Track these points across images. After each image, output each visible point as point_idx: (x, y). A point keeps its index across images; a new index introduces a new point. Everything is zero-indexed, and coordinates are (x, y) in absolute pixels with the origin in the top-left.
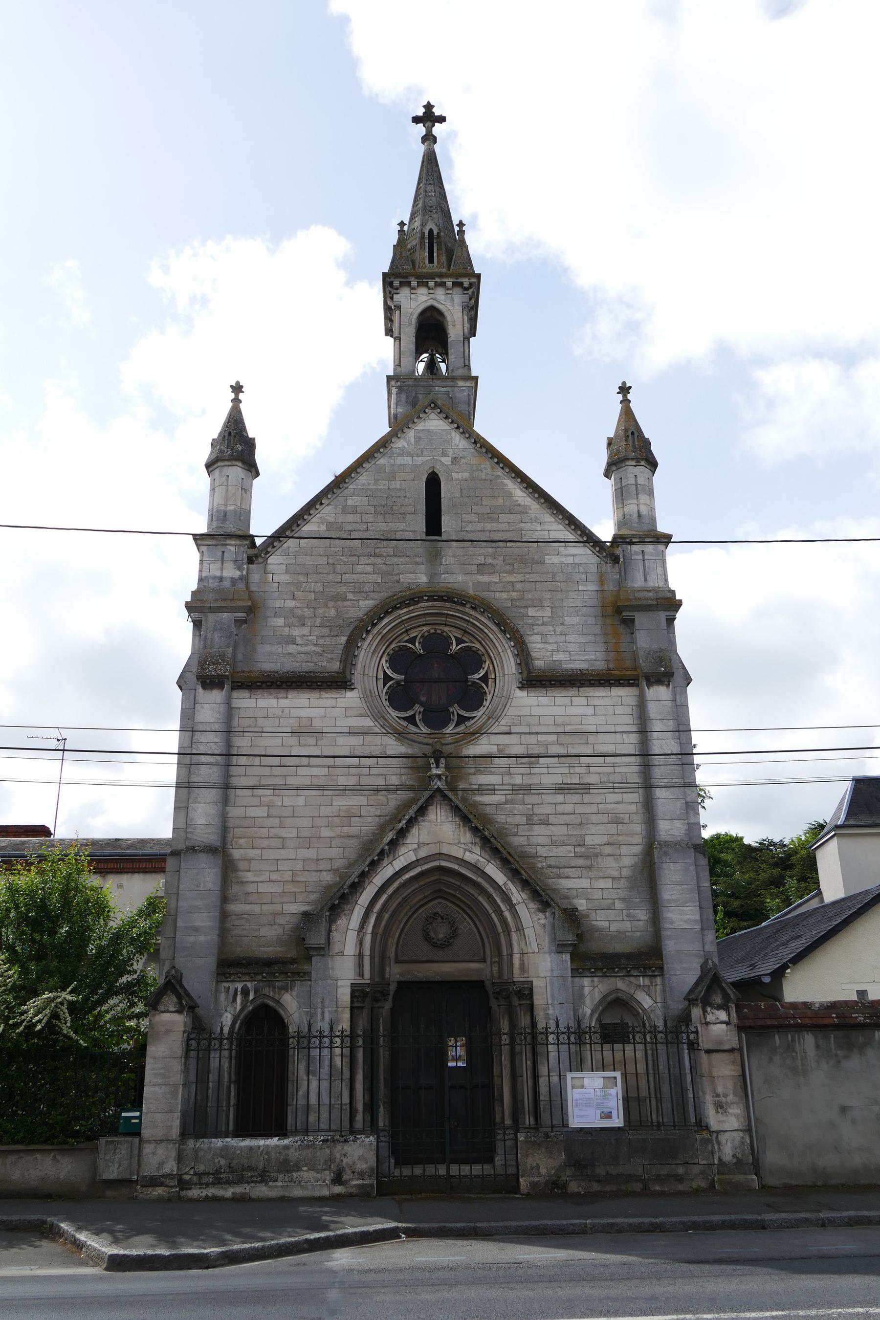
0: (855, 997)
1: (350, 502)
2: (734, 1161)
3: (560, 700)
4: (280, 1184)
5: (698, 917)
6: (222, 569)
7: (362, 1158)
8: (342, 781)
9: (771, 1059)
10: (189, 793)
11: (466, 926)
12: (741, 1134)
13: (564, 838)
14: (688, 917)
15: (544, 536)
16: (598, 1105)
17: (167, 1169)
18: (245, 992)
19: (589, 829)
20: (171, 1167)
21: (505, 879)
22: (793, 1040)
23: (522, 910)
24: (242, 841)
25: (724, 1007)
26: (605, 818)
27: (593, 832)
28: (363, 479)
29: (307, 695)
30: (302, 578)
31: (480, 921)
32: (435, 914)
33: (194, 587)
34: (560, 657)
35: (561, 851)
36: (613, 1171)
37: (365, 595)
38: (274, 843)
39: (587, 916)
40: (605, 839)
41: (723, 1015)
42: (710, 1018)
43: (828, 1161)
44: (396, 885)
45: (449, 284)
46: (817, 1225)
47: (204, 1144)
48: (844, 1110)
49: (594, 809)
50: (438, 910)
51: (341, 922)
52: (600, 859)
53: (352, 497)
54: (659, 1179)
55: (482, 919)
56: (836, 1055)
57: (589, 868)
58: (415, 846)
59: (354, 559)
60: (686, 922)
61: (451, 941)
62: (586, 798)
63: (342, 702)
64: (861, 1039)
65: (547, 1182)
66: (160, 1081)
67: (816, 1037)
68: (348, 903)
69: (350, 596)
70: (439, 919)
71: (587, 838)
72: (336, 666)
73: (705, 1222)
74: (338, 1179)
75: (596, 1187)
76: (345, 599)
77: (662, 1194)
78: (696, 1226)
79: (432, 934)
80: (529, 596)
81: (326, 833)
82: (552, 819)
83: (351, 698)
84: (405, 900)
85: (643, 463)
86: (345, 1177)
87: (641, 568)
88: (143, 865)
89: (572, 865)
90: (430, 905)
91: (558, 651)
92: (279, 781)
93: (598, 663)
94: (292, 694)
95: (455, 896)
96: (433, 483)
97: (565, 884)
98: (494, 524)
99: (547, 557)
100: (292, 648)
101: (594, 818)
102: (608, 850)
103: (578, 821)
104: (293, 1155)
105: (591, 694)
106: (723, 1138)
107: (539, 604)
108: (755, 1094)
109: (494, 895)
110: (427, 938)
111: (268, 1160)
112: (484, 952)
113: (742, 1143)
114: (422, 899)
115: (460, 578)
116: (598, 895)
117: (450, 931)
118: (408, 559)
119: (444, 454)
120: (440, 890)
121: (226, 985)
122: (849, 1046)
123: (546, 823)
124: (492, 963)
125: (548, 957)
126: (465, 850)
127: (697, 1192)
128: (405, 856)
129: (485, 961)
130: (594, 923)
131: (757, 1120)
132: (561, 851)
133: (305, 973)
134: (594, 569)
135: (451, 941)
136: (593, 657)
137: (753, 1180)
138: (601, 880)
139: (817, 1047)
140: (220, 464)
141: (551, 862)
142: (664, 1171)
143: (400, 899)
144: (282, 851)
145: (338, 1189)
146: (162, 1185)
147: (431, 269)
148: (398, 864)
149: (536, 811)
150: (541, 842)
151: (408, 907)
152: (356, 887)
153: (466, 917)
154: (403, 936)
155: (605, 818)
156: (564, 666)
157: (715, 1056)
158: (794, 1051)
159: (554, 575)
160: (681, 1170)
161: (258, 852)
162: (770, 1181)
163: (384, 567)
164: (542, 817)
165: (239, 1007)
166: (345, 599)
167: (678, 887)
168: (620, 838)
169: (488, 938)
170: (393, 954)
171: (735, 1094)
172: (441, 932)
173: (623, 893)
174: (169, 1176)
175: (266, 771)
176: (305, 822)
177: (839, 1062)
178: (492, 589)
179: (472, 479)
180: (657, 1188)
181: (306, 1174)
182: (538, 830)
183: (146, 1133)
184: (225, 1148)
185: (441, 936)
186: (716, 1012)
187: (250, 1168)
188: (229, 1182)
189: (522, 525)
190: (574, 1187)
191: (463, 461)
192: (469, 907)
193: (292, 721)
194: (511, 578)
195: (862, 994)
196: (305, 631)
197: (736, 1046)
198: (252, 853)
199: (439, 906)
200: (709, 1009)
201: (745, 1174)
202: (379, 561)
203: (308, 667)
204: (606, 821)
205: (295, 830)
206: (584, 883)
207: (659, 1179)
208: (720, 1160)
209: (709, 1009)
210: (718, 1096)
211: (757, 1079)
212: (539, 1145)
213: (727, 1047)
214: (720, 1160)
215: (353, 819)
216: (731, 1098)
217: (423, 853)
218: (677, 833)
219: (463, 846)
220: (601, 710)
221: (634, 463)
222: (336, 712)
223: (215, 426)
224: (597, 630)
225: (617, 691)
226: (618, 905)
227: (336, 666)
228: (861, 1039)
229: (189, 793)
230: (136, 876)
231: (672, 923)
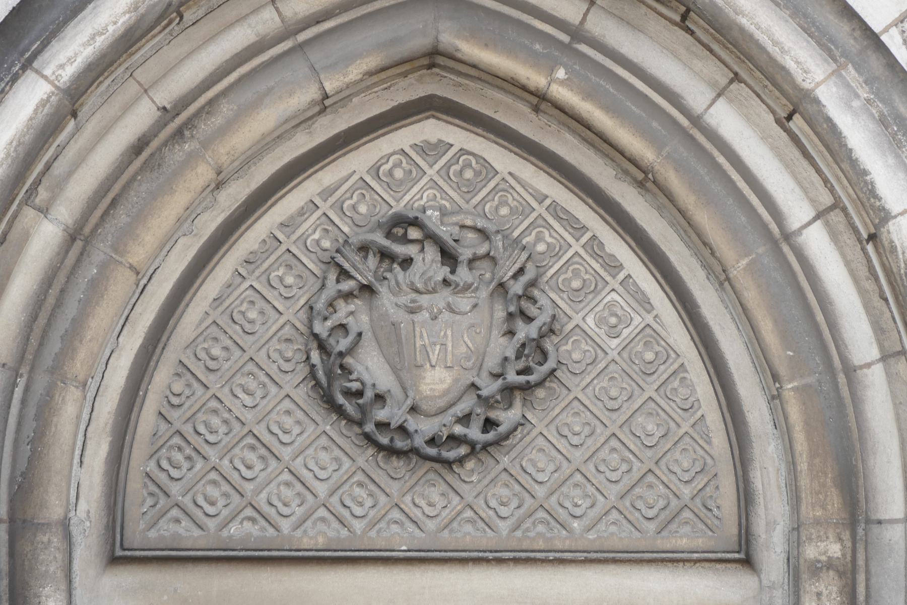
10: (135, 79)
11: (611, 310)
31: (722, 278)
32: (400, 224)
50: (415, 198)
55: (738, 267)
61: (507, 417)
70: (428, 262)
79: (372, 368)
84: (179, 123)
90: (358, 161)
95: (540, 101)
109: (830, 100)
110: (336, 392)
112: (746, 497)
114: (302, 121)
117: (500, 347)
120: (435, 58)
124: (797, 572)
129: (748, 562)
135: (507, 417)
143: (141, 117)
151: (203, 174)
153: (617, 246)
154: (162, 376)
169: (775, 399)
170: (88, 508)
172: (439, 350)
185: (436, 382)
192: (645, 179)
199: (421, 168)
229: (135, 79)
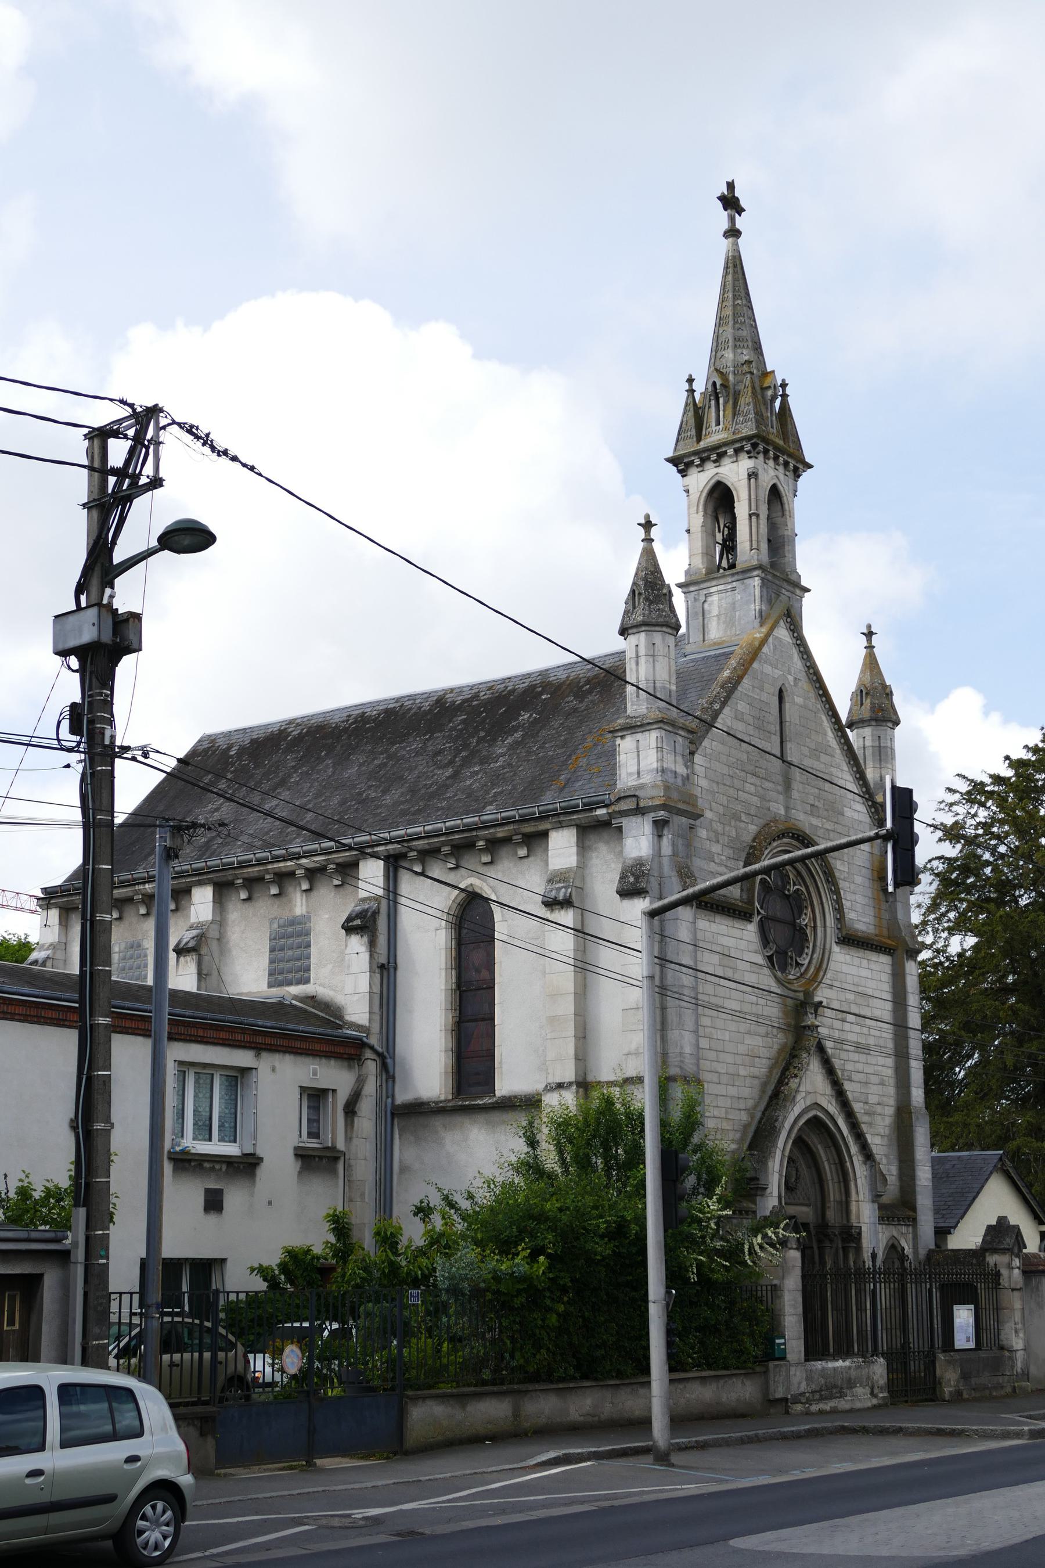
15: (840, 782)
17: (802, 1389)
47: (819, 1365)
86: (876, 1391)
88: (298, 1044)
94: (719, 918)
103: (864, 1080)
104: (853, 1373)
133: (747, 1212)
140: (664, 629)
145: (875, 1401)
147: (743, 424)
174: (803, 1394)
183: (789, 1357)
187: (835, 1386)
190: (965, 1396)
225: (873, 956)
230: (288, 1058)
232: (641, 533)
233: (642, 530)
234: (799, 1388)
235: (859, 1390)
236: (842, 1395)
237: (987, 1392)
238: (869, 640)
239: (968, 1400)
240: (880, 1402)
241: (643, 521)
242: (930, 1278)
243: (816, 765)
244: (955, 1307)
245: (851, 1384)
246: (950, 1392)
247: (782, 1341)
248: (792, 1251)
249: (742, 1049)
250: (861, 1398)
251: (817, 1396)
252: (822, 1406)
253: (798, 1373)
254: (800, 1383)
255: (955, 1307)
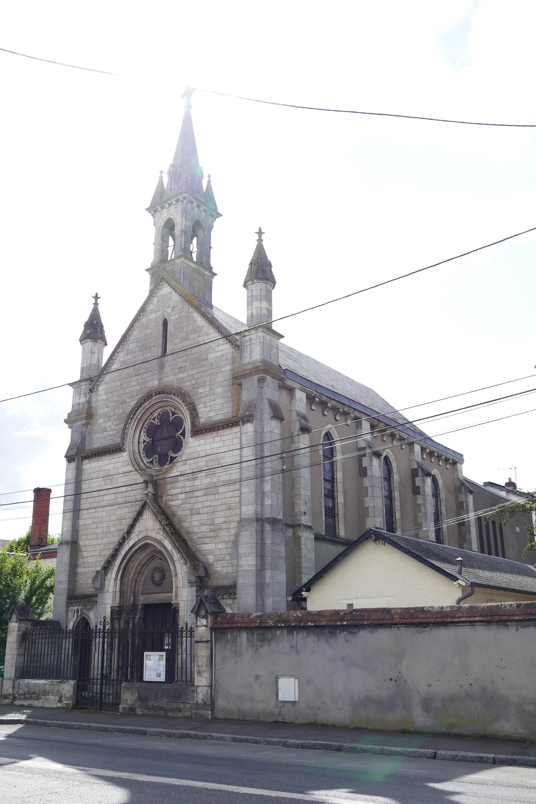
0: (345, 608)
1: (130, 348)
2: (203, 702)
3: (210, 440)
4: (42, 701)
5: (255, 563)
6: (80, 399)
7: (68, 691)
8: (119, 500)
9: (225, 647)
12: (206, 688)
13: (205, 521)
14: (250, 563)
16: (156, 669)
17: (9, 692)
18: (78, 612)
19: (217, 514)
20: (10, 691)
21: (172, 547)
22: (237, 636)
23: (177, 564)
24: (83, 537)
25: (205, 617)
26: (224, 507)
27: (218, 516)
28: (136, 333)
29: (108, 458)
30: (110, 395)
33: (70, 410)
34: (211, 414)
35: (204, 528)
36: (155, 704)
37: (133, 398)
38: (94, 536)
39: (213, 565)
40: (223, 520)
41: (204, 622)
42: (199, 623)
43: (247, 706)
44: (129, 555)
45: (174, 202)
46: (167, 736)
48: (257, 677)
49: (219, 502)
51: (109, 575)
52: (221, 531)
53: (131, 345)
54: (172, 710)
56: (257, 645)
57: (215, 537)
58: (138, 533)
59: (129, 379)
60: (249, 566)
62: (217, 496)
63: (122, 459)
64: (270, 636)
65: (129, 708)
66: (10, 653)
67: (248, 634)
68: (111, 565)
69: (128, 400)
71: (216, 520)
72: (118, 440)
73: (124, 729)
74: (60, 701)
75: (147, 712)
76: (126, 402)
77: (173, 717)
78: (119, 731)
80: (200, 381)
81: (113, 529)
82: (201, 511)
83: (124, 457)
85: (255, 281)
86: (63, 699)
87: (249, 350)
89: (208, 536)
91: (211, 411)
92: (96, 505)
93: (229, 414)
96: (165, 323)
97: (205, 547)
98: (187, 342)
99: (209, 355)
100: (106, 434)
101: (219, 508)
102: (225, 526)
103: (212, 511)
104: (48, 688)
105: (223, 434)
106: (199, 690)
107: (203, 385)
108: (217, 666)
111: (40, 690)
113: (207, 693)
115: (171, 378)
116: (218, 552)
118: (151, 373)
119: (169, 307)
121: (71, 608)
122: (263, 639)
123: (198, 513)
125: (186, 590)
126: (157, 533)
127: (187, 718)
128: (134, 539)
130: (216, 569)
131: (215, 681)
132: (204, 528)
134: (230, 356)
136: (226, 411)
137: (209, 714)
138: (221, 544)
139: (248, 640)
141: (200, 535)
142: (175, 706)
144: (97, 540)
145: (59, 705)
146: (8, 698)
148: (131, 543)
149: (195, 507)
150: (194, 524)
152: (114, 556)
155: (224, 507)
156: (214, 419)
157: (199, 644)
158: (237, 642)
159: (212, 364)
160: (182, 706)
161: (88, 541)
162: (219, 715)
163: (141, 380)
164: (197, 510)
165: (75, 619)
166: (126, 402)
167: (247, 546)
168: (231, 518)
171: (206, 666)
173: (230, 551)
174: (9, 694)
175: (92, 500)
176: (105, 525)
177: (258, 649)
178: (184, 381)
179: (179, 317)
180: (170, 715)
181: (51, 697)
182: (196, 517)
183: (5, 675)
184: (28, 684)
186: (201, 619)
187: (34, 693)
188: (28, 699)
189: (200, 338)
190: (138, 711)
191: (176, 308)
193: (103, 472)
194: (192, 372)
195: (350, 605)
196: (110, 424)
197: (209, 639)
198: (87, 542)
200: (198, 618)
201: (206, 710)
202: (139, 377)
203: (110, 442)
204: (225, 508)
205: (101, 529)
206: (211, 546)
207: (172, 710)
208: (197, 702)
209: (198, 618)
210: (199, 666)
211: (218, 658)
212: (128, 688)
213: (205, 640)
214: (197, 702)
215: (123, 521)
216: (204, 668)
217: (140, 537)
218: (250, 513)
219: (156, 531)
220: (227, 443)
221: (251, 283)
222: (119, 465)
223: (248, 255)
224: (229, 394)
226: (227, 558)
227: (118, 440)
228: (270, 636)
231: (242, 567)
232: (93, 300)
233: (94, 299)
234: (7, 691)
235: (51, 697)
236: (38, 698)
237: (162, 713)
238: (96, 301)
239: (138, 715)
240: (64, 706)
241: (258, 231)
242: (104, 635)
243: (191, 342)
244: (146, 653)
245: (45, 693)
246: (124, 708)
247: (3, 667)
248: (13, 623)
249: (113, 518)
250: (52, 702)
251: (22, 697)
252: (22, 702)
253: (8, 684)
254: (8, 689)
255: (146, 653)
